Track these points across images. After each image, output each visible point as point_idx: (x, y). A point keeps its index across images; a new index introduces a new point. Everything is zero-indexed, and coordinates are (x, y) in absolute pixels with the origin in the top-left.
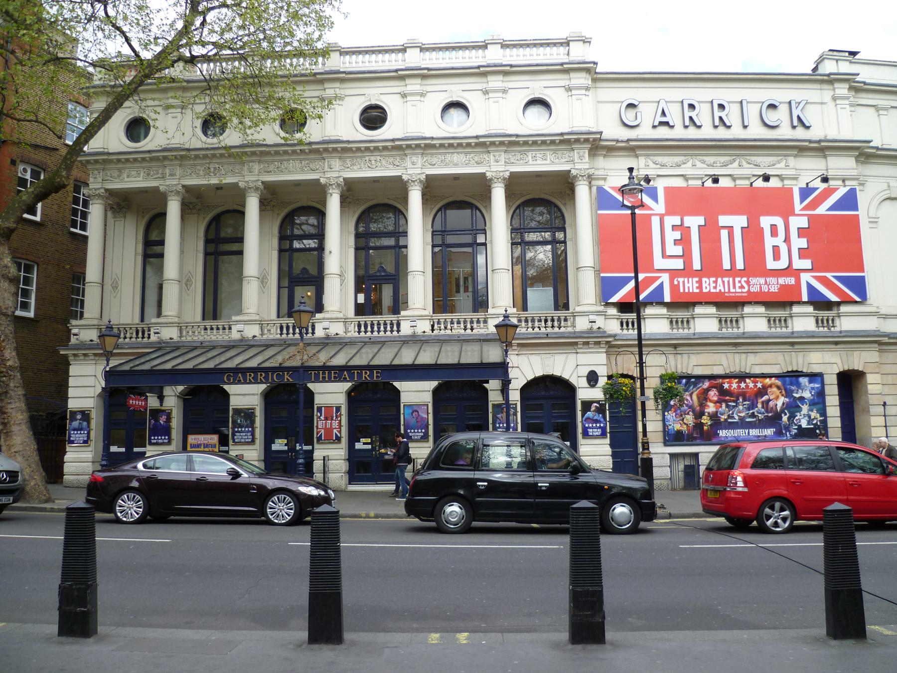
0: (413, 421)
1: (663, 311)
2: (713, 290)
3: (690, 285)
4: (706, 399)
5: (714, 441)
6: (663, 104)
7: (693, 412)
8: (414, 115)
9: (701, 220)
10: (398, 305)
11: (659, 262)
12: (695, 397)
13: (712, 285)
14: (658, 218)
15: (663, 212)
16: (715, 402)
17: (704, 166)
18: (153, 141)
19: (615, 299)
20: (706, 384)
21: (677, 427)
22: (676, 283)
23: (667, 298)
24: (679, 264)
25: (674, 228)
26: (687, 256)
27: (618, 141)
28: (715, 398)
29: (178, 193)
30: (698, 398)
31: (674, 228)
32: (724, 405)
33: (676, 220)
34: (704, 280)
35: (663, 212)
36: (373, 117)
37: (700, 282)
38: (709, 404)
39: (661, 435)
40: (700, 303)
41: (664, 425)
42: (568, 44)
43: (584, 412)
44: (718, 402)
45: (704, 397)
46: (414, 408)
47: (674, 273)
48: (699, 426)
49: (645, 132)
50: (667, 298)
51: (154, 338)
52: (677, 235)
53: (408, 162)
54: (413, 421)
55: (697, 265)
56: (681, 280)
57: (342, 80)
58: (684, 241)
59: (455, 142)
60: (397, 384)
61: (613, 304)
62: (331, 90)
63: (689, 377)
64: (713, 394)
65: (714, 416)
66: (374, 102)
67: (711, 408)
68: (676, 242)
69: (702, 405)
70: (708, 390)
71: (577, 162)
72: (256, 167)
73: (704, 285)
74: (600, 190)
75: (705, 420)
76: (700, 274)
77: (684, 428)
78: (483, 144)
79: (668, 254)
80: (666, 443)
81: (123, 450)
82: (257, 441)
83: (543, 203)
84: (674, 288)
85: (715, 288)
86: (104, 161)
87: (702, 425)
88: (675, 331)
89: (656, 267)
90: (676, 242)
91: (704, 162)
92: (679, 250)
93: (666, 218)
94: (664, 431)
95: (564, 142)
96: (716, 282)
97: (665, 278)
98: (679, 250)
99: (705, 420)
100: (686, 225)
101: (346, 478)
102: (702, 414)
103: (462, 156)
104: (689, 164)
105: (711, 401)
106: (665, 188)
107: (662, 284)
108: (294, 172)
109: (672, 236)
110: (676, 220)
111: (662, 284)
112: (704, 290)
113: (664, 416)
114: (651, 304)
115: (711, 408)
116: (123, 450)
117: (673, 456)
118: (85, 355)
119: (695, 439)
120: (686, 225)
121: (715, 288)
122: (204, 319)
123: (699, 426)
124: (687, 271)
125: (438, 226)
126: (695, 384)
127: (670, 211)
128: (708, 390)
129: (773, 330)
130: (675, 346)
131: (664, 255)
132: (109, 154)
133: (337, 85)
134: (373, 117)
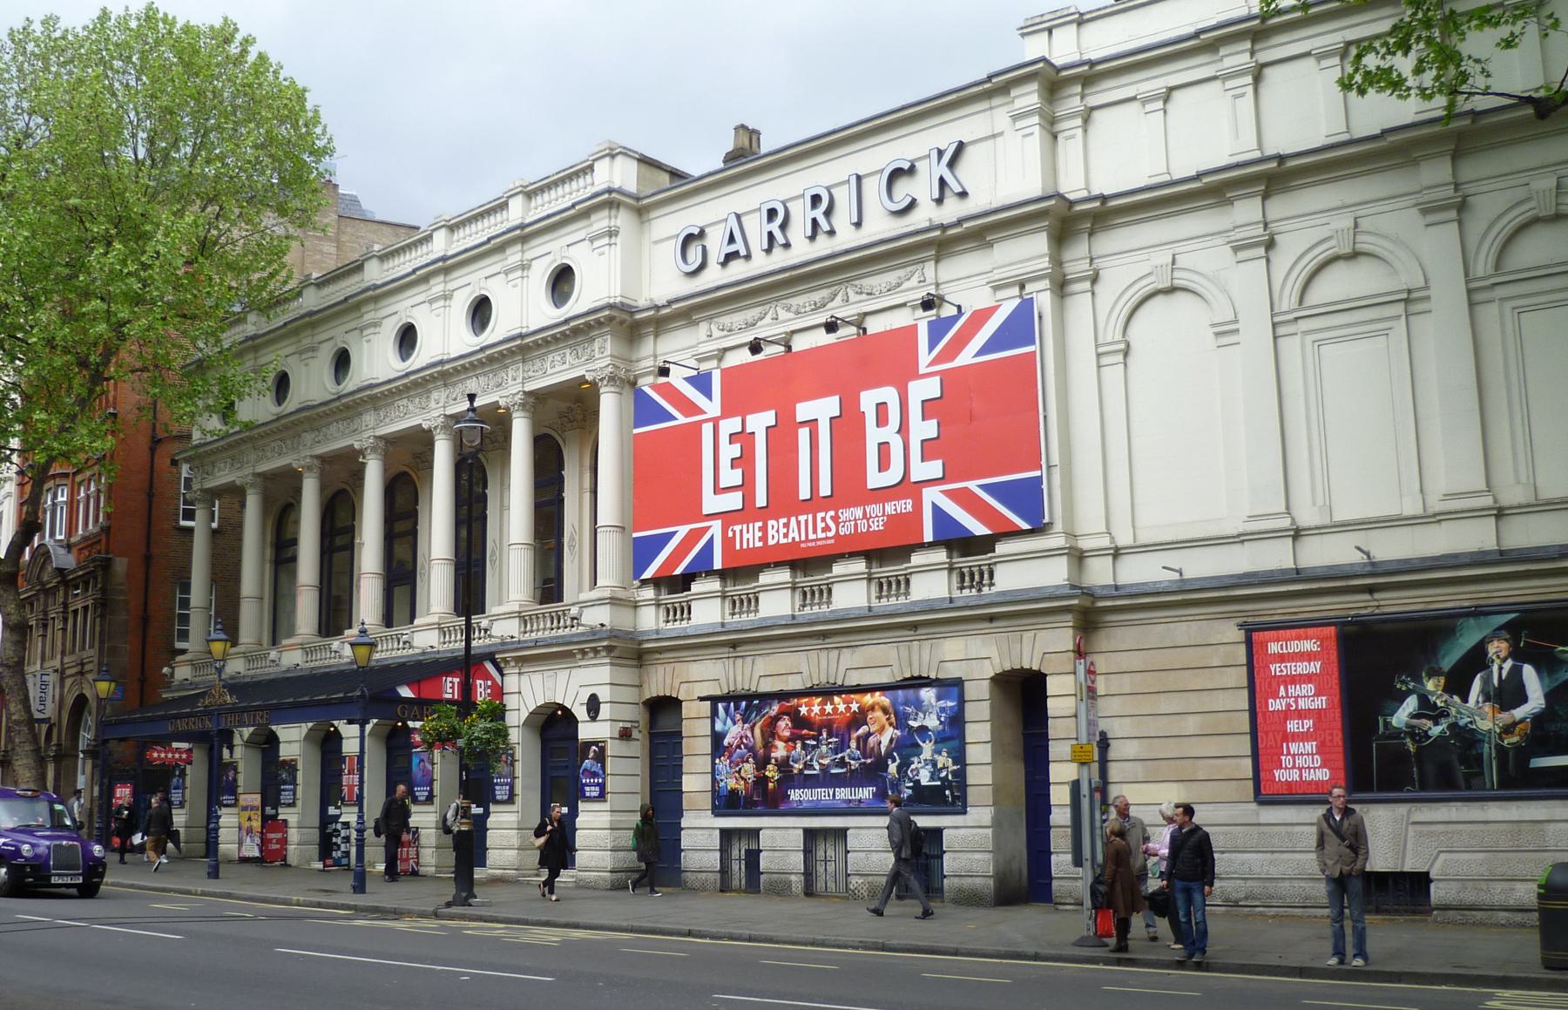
1: (714, 585)
2: (783, 541)
3: (749, 536)
9: (768, 418)
11: (712, 503)
12: (757, 731)
16: (786, 741)
19: (648, 574)
21: (731, 784)
23: (718, 565)
24: (734, 501)
25: (733, 438)
26: (747, 486)
28: (787, 734)
37: (764, 529)
41: (714, 780)
45: (770, 732)
47: (728, 517)
48: (761, 781)
52: (735, 451)
55: (761, 500)
56: (737, 528)
58: (744, 462)
63: (749, 697)
64: (784, 726)
65: (783, 765)
67: (780, 750)
69: (768, 746)
70: (777, 718)
72: (308, 438)
73: (771, 532)
77: (741, 786)
80: (717, 811)
84: (728, 543)
85: (786, 535)
87: (766, 779)
91: (789, 310)
93: (722, 423)
94: (713, 791)
96: (787, 525)
97: (716, 527)
99: (771, 772)
100: (749, 430)
104: (768, 320)
105: (780, 739)
110: (731, 425)
113: (713, 764)
117: (726, 834)
119: (756, 804)
120: (749, 430)
121: (786, 535)
123: (761, 781)
124: (747, 513)
126: (759, 709)
127: (727, 412)
128: (777, 718)
130: (734, 645)
131: (717, 490)
133: (372, 306)
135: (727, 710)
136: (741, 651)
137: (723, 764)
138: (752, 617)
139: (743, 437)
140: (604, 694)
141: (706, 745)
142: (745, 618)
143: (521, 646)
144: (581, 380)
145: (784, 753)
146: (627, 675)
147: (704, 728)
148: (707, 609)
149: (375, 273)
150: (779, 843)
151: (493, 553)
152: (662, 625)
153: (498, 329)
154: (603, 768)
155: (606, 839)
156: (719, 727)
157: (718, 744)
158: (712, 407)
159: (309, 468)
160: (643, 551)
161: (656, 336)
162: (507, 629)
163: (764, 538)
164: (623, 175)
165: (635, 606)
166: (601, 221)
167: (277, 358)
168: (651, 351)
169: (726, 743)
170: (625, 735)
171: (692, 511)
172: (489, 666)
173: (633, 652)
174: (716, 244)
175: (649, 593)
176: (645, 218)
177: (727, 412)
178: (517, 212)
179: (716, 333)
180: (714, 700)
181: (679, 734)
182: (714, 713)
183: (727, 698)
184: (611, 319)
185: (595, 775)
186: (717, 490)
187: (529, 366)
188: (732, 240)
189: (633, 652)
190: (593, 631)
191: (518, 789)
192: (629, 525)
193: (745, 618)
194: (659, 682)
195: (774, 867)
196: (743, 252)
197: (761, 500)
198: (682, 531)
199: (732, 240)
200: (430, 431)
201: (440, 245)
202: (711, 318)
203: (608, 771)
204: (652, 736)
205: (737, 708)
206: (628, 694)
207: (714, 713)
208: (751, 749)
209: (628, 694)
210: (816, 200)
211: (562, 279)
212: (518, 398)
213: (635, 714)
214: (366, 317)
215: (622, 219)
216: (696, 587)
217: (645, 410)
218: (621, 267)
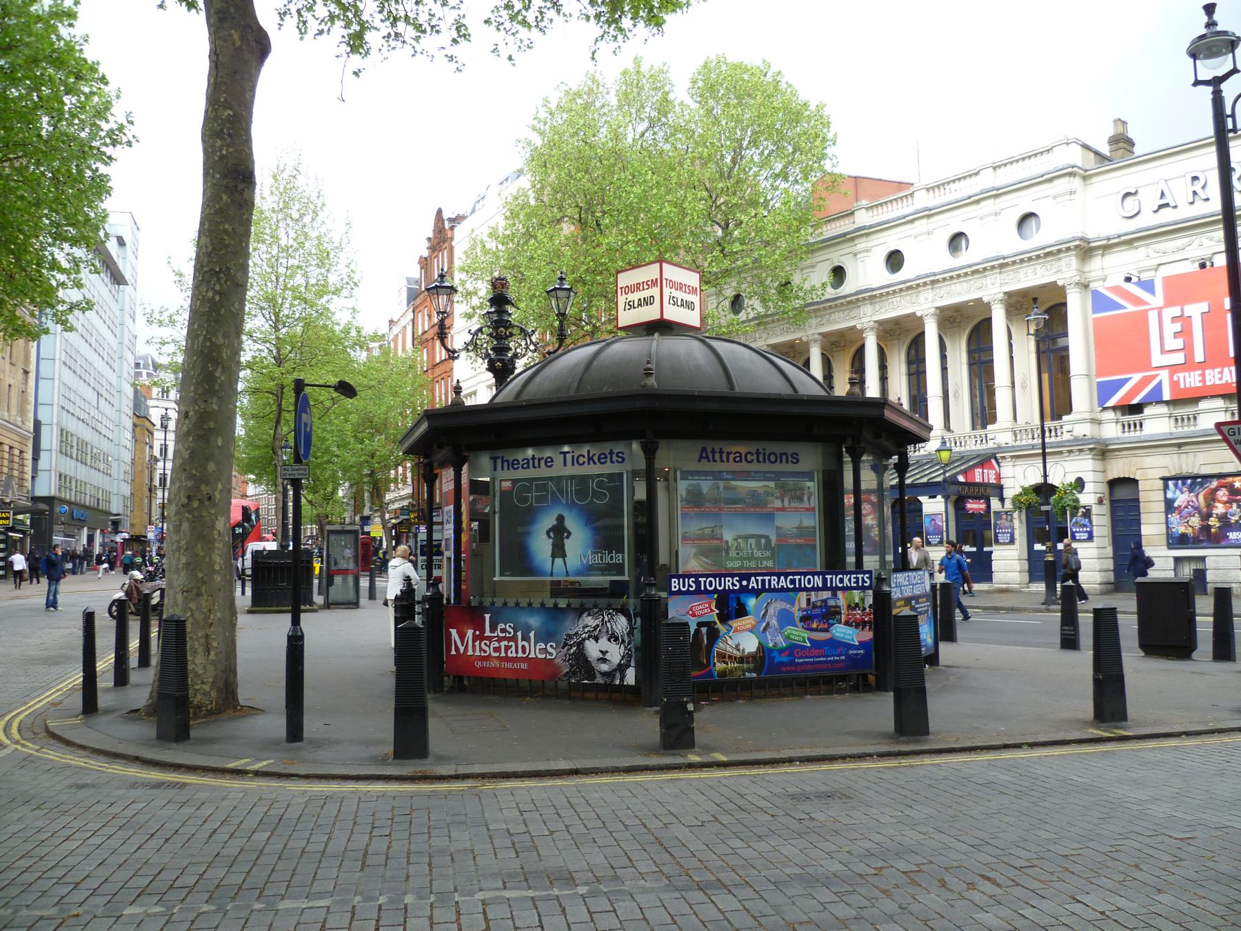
0: (932, 529)
1: (1164, 409)
2: (1218, 382)
3: (1191, 380)
4: (1214, 500)
5: (1223, 543)
6: (1163, 186)
7: (1200, 513)
8: (926, 252)
9: (1204, 307)
10: (993, 419)
11: (1157, 359)
12: (1201, 497)
13: (1218, 376)
14: (1156, 312)
15: (1161, 304)
16: (1225, 503)
17: (1213, 243)
18: (848, 287)
19: (1111, 403)
20: (1215, 484)
21: (1182, 530)
22: (1175, 379)
23: (1166, 396)
24: (1179, 358)
25: (1174, 319)
26: (1188, 349)
27: (1109, 239)
28: (1225, 499)
29: (872, 329)
30: (1205, 499)
31: (1174, 319)
32: (1235, 505)
33: (1176, 311)
34: (1207, 372)
35: (1161, 304)
36: (895, 260)
37: (1203, 375)
38: (1217, 504)
39: (1164, 538)
40: (1205, 397)
41: (1168, 527)
42: (852, 213)
43: (1072, 516)
44: (1229, 502)
45: (1212, 498)
46: (933, 517)
47: (1173, 369)
48: (1206, 528)
49: (1148, 220)
50: (1166, 396)
51: (1067, 436)
52: (1178, 327)
53: (922, 296)
54: (932, 529)
55: (1199, 356)
56: (1181, 375)
57: (868, 235)
58: (1185, 332)
59: (903, 286)
60: (920, 498)
61: (1114, 408)
62: (861, 244)
63: (1194, 477)
64: (1223, 494)
65: (1223, 518)
66: (893, 248)
67: (1220, 509)
68: (1176, 335)
69: (1210, 506)
70: (1217, 489)
71: (1064, 272)
72: (814, 322)
73: (1208, 378)
74: (1095, 293)
75: (1213, 522)
76: (1203, 366)
77: (1190, 531)
78: (978, 271)
79: (1167, 348)
80: (1170, 546)
81: (974, 549)
82: (1017, 542)
83: (1046, 313)
84: (1174, 385)
85: (1221, 379)
86: (871, 297)
87: (1210, 527)
88: (1126, 434)
89: (1154, 365)
90: (1176, 335)
91: (1212, 239)
92: (1179, 343)
93: (1164, 311)
94: (1168, 534)
95: (1051, 254)
96: (1221, 373)
97: (1164, 376)
98: (1179, 343)
99: (1213, 522)
100: (1186, 314)
101: (1026, 577)
102: (1209, 515)
103: (964, 284)
104: (1195, 245)
105: (1220, 502)
106: (1152, 281)
107: (1160, 384)
108: (839, 322)
109: (1171, 328)
110: (1176, 311)
111: (1160, 384)
112: (1208, 383)
113: (1167, 518)
114: (1151, 403)
115: (1220, 509)
116: (974, 549)
117: (1178, 560)
118: (1070, 452)
119: (1202, 541)
120: (1186, 314)
121: (1221, 379)
122: (974, 428)
123: (1206, 528)
124: (1189, 365)
125: (913, 358)
126: (1202, 484)
127: (1169, 302)
128: (1217, 489)
129: (1180, 429)
130: (1179, 446)
131: (1163, 351)
132: (872, 290)
133: (864, 239)
134: (895, 260)
135: (1176, 485)
136: (1185, 449)
137: (1174, 518)
138: (1192, 428)
139: (1185, 321)
140: (1087, 477)
141: (1161, 506)
142: (1187, 429)
143: (1014, 449)
144: (979, 301)
145: (1223, 511)
146: (1098, 465)
147: (1160, 496)
148: (1157, 423)
149: (863, 218)
150: (1221, 565)
151: (956, 392)
152: (1120, 435)
153: (967, 257)
154: (1091, 522)
155: (1097, 565)
156: (1170, 495)
157: (1169, 505)
158: (1157, 300)
159: (815, 341)
160: (1105, 391)
161: (1103, 255)
162: (1005, 439)
163: (1204, 380)
164: (1075, 156)
165: (1100, 423)
166: (1063, 184)
167: (837, 256)
168: (1097, 265)
169: (1176, 505)
170: (1100, 501)
171: (1144, 362)
172: (993, 461)
173: (1103, 451)
174: (1149, 199)
175: (1110, 415)
176: (1088, 182)
177: (1169, 302)
178: (988, 180)
179: (1153, 254)
180: (1165, 480)
181: (1137, 500)
182: (1166, 487)
183: (1175, 478)
184: (1077, 247)
185: (1084, 526)
186: (1163, 351)
187: (1005, 276)
188: (1163, 194)
189: (1103, 451)
190: (1076, 439)
191: (1017, 535)
192: (1094, 372)
193: (1133, 435)
194: (1118, 469)
195: (1218, 579)
196: (1172, 204)
197: (1199, 356)
198: (1136, 377)
199: (1163, 194)
200: (1063, 288)
201: (922, 200)
202: (1148, 245)
203: (1094, 523)
204: (1112, 502)
205: (1184, 484)
206: (1100, 477)
207: (1166, 487)
208: (1197, 508)
209: (1100, 477)
210: (1195, 178)
211: (956, 241)
212: (932, 310)
213: (1104, 489)
214: (859, 247)
215: (1076, 183)
216: (1148, 411)
217: (1101, 303)
218: (1074, 212)
